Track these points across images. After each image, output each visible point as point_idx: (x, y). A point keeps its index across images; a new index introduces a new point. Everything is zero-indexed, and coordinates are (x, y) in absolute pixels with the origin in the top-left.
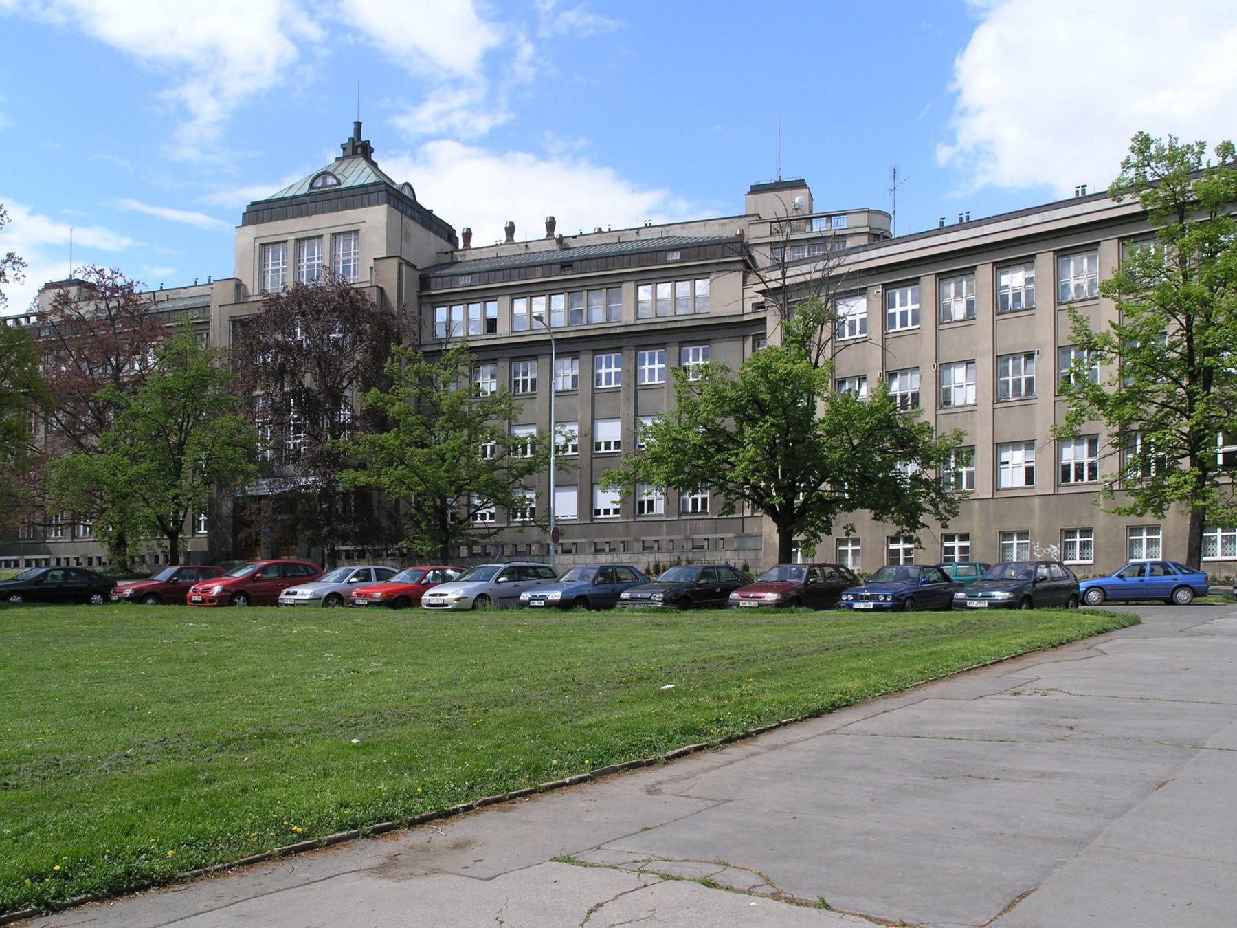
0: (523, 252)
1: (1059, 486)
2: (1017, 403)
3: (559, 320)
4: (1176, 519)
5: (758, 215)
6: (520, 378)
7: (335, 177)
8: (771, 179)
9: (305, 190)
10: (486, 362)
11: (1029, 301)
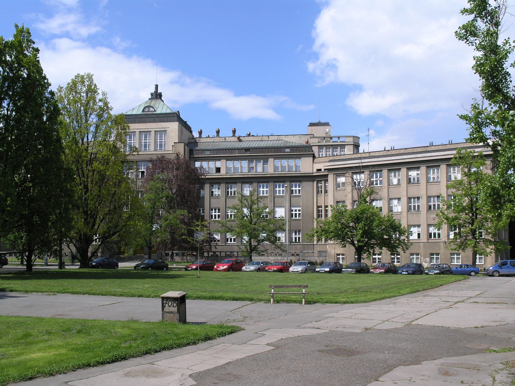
0: (224, 141)
1: (428, 239)
2: (415, 213)
3: (246, 170)
4: (469, 252)
5: (313, 135)
6: (229, 190)
7: (153, 108)
8: (316, 121)
9: (140, 112)
10: (216, 183)
11: (418, 181)
